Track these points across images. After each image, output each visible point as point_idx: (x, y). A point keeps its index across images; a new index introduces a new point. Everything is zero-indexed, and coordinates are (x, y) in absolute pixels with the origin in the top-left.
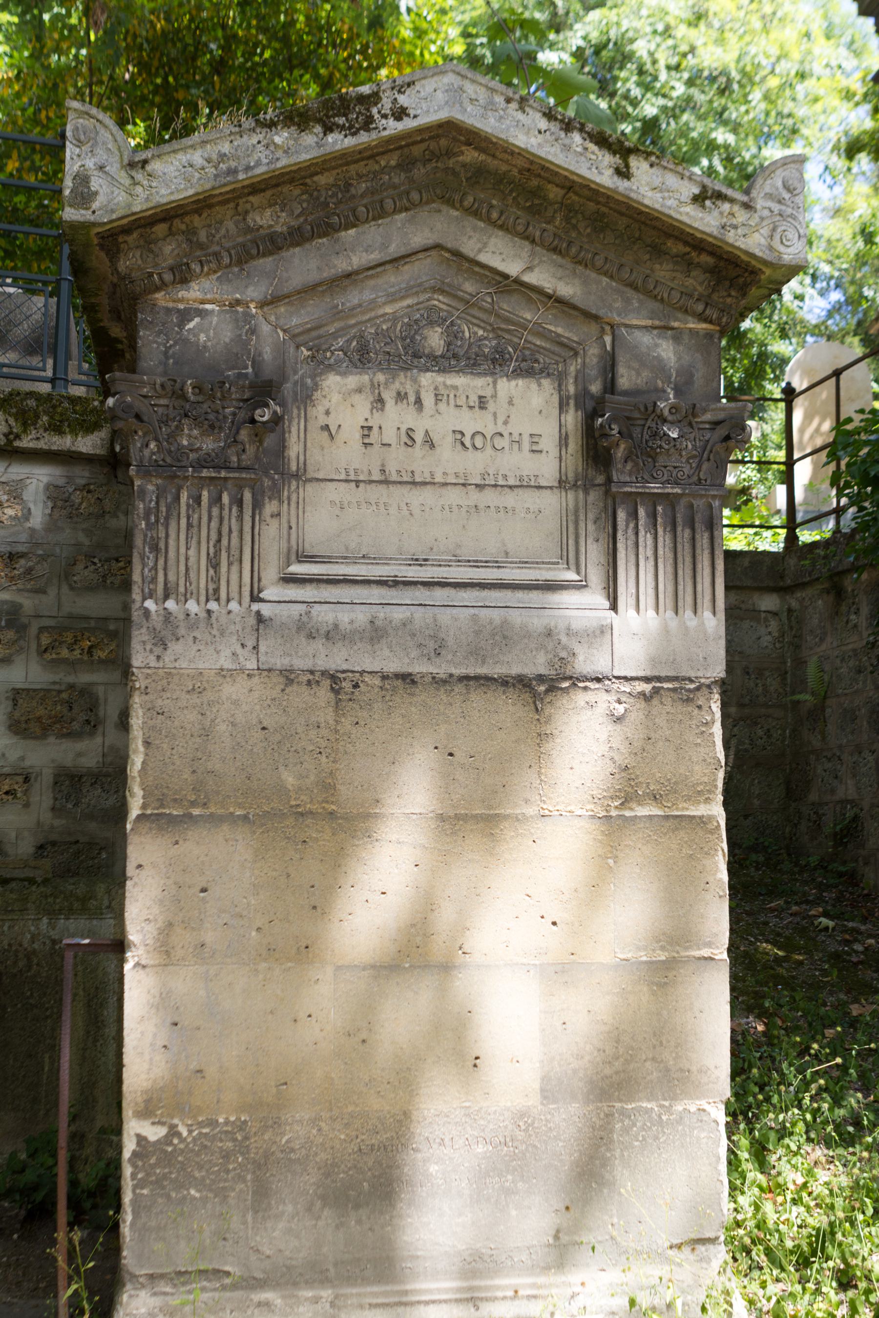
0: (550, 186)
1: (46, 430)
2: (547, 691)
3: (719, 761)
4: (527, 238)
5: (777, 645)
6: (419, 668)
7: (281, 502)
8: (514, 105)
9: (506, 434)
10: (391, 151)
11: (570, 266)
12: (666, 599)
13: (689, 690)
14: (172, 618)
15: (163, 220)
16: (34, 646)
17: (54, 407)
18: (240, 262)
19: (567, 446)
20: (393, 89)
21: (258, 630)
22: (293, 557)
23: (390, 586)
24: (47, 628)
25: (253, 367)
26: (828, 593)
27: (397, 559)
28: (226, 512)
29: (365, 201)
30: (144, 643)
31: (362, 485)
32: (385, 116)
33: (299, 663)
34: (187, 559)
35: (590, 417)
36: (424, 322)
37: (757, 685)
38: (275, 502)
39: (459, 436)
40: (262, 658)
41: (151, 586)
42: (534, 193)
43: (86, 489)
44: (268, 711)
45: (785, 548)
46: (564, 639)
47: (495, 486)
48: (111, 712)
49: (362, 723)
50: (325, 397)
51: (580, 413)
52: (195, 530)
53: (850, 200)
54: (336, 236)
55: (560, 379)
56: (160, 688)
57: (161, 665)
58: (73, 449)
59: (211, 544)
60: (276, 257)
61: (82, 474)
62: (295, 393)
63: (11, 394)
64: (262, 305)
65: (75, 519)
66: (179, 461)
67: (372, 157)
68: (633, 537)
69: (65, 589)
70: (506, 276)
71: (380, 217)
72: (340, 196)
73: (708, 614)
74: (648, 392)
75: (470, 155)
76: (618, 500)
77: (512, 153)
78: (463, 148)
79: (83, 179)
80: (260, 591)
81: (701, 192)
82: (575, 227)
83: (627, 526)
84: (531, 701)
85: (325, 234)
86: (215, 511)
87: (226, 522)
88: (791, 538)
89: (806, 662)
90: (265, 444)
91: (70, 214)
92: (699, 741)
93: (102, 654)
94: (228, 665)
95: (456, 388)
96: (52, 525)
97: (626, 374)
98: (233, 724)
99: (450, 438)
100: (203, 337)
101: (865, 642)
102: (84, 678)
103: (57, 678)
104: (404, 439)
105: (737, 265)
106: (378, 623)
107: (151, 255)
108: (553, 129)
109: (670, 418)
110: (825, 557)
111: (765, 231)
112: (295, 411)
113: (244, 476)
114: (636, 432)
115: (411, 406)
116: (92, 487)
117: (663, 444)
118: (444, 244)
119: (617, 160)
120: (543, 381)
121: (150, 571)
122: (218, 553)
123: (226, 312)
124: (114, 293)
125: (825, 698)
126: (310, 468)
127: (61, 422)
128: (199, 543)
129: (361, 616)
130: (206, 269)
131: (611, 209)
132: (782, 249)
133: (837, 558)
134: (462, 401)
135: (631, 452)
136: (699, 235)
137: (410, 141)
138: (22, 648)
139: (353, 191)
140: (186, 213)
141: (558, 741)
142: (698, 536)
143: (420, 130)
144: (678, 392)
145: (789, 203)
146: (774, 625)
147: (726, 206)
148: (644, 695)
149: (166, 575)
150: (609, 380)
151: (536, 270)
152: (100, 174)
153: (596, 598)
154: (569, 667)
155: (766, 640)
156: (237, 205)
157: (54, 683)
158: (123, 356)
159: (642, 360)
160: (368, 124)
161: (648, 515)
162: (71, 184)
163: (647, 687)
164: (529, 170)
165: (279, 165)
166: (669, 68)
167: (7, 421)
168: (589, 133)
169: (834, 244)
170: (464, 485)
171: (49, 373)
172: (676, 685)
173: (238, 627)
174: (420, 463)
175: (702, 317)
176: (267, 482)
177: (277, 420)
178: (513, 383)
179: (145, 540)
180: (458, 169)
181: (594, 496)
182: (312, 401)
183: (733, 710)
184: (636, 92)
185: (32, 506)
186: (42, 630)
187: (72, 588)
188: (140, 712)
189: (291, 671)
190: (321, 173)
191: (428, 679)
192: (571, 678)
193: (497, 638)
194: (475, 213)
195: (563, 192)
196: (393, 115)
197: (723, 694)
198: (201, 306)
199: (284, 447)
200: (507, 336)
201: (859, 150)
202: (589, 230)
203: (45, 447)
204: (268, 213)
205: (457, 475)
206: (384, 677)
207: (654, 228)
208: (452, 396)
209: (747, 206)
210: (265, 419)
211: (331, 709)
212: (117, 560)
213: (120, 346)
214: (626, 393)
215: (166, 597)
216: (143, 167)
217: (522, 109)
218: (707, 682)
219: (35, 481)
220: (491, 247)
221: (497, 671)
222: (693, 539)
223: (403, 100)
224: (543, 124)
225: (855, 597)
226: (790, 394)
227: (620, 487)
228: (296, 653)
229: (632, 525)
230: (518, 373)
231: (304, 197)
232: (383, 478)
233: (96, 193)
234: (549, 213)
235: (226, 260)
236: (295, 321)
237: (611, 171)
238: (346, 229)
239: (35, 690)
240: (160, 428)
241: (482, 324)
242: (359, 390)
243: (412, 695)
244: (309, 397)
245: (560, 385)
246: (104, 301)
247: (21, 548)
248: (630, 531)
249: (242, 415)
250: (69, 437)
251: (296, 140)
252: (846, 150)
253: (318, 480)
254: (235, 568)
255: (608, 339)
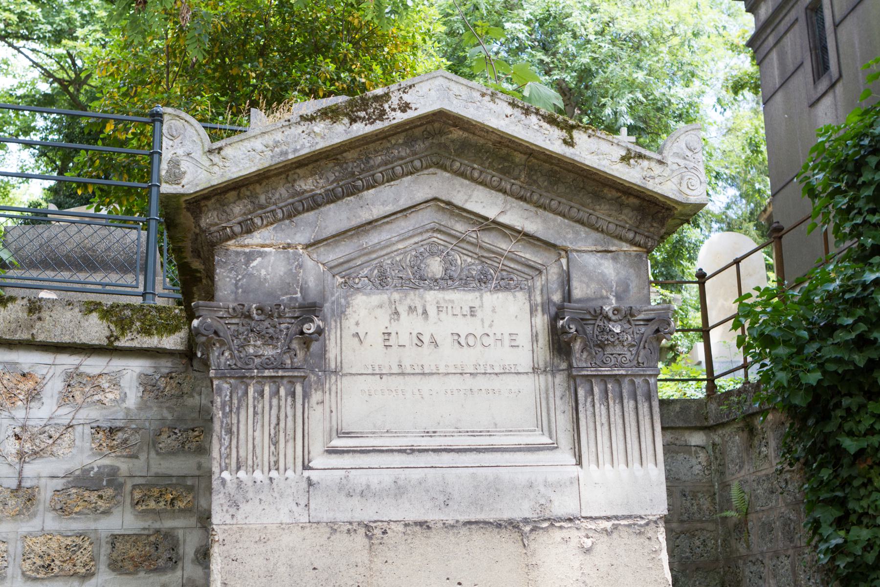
0: (516, 153)
1: (138, 333)
2: (532, 530)
3: (667, 580)
4: (500, 191)
5: (706, 472)
6: (430, 516)
7: (324, 392)
8: (487, 98)
9: (491, 334)
10: (399, 133)
11: (533, 209)
12: (619, 455)
13: (641, 526)
14: (243, 486)
15: (234, 189)
16: (128, 500)
17: (145, 315)
18: (290, 216)
19: (537, 341)
20: (399, 90)
21: (308, 492)
22: (334, 434)
23: (408, 454)
24: (138, 485)
25: (301, 293)
26: (743, 431)
27: (412, 433)
28: (283, 403)
29: (381, 169)
30: (222, 505)
31: (384, 377)
32: (394, 110)
33: (341, 517)
34: (254, 439)
35: (554, 320)
36: (427, 254)
37: (692, 505)
38: (319, 393)
39: (456, 337)
40: (312, 514)
41: (227, 461)
42: (505, 158)
43: (169, 376)
44: (318, 555)
45: (708, 396)
46: (542, 490)
47: (485, 373)
48: (189, 546)
49: (390, 562)
50: (355, 312)
51: (546, 316)
52: (259, 417)
53: (738, 122)
54: (360, 194)
55: (530, 291)
56: (234, 540)
57: (235, 521)
58: (160, 346)
59: (272, 426)
60: (317, 211)
61: (166, 365)
62: (333, 311)
63: (112, 307)
64: (307, 246)
65: (161, 400)
66: (247, 365)
67: (386, 138)
68: (591, 409)
69: (153, 454)
70: (486, 219)
71: (392, 180)
72: (362, 166)
73: (651, 466)
74: (596, 299)
75: (457, 134)
76: (578, 381)
77: (487, 132)
78: (452, 129)
79: (175, 163)
80: (309, 462)
81: (627, 154)
82: (535, 182)
83: (586, 401)
84: (519, 539)
85: (352, 194)
86: (275, 402)
87: (283, 409)
88: (711, 387)
89: (729, 485)
90: (311, 349)
91: (166, 188)
92: (651, 565)
93: (182, 505)
94: (286, 519)
95: (452, 301)
96: (143, 406)
97: (579, 287)
98: (291, 566)
99: (450, 339)
100: (263, 272)
101: (774, 469)
102: (168, 524)
103: (146, 525)
104: (416, 341)
105: (656, 205)
106: (400, 483)
107: (225, 214)
108: (516, 114)
109: (614, 318)
110: (739, 403)
111: (675, 180)
112: (333, 323)
113: (296, 374)
114: (589, 329)
115: (420, 316)
116: (173, 374)
117: (609, 337)
118: (440, 197)
119: (564, 134)
120: (517, 294)
121: (226, 449)
122: (277, 433)
123: (281, 253)
124: (196, 239)
125: (747, 514)
126: (345, 366)
127: (150, 326)
128: (263, 426)
129: (387, 477)
130: (265, 222)
131: (561, 167)
132: (688, 192)
133: (748, 403)
134: (457, 311)
135: (586, 345)
136: (627, 185)
137: (412, 125)
138: (119, 502)
139: (372, 162)
140: (251, 184)
141: (542, 569)
142: (640, 406)
143: (420, 118)
144: (618, 297)
145: (691, 159)
146: (702, 456)
147: (645, 163)
148: (606, 531)
149: (238, 452)
150: (566, 291)
151: (509, 213)
152: (188, 159)
153: (566, 456)
154: (547, 511)
155: (697, 469)
156: (288, 176)
157: (144, 529)
158: (201, 281)
159: (589, 276)
160: (382, 115)
161: (601, 391)
162: (166, 167)
163: (608, 525)
164: (500, 143)
165: (318, 147)
166: (596, 33)
167: (109, 327)
168: (542, 116)
169: (728, 154)
170: (461, 374)
171: (141, 289)
172: (631, 522)
173: (294, 490)
174: (427, 358)
175: (632, 243)
176: (313, 378)
177: (320, 332)
178: (495, 296)
179: (222, 426)
180: (448, 143)
181: (560, 378)
182: (345, 315)
183: (674, 525)
184: (572, 49)
185: (127, 390)
186: (134, 487)
187: (158, 454)
188: (219, 559)
189: (335, 523)
190: (349, 151)
191: (440, 525)
192: (549, 519)
193: (491, 490)
194: (463, 175)
195: (526, 157)
196: (400, 108)
197: (669, 531)
198: (262, 249)
199: (325, 351)
200: (489, 262)
201: (743, 87)
202: (546, 184)
203: (138, 346)
204: (310, 181)
205: (455, 367)
206: (406, 525)
207: (594, 180)
208: (450, 308)
209: (661, 162)
210: (311, 331)
211: (366, 552)
212: (193, 430)
213: (199, 275)
214: (579, 301)
215: (238, 469)
216: (219, 153)
217: (493, 100)
218: (654, 518)
219: (129, 371)
220: (474, 198)
221: (492, 516)
222: (637, 408)
223: (407, 98)
224: (509, 110)
225: (764, 433)
226: (702, 277)
227: (579, 371)
228: (338, 508)
229: (589, 400)
230: (498, 289)
231: (337, 168)
232: (400, 371)
233: (184, 173)
234: (516, 173)
235: (280, 215)
236: (332, 257)
237: (561, 141)
238: (368, 189)
239: (129, 535)
240: (233, 341)
241: (470, 254)
242: (381, 306)
243: (428, 537)
244: (343, 312)
245: (530, 297)
246: (188, 245)
247: (119, 424)
248: (588, 404)
249: (294, 329)
250: (156, 337)
251: (329, 129)
252: (732, 87)
253: (351, 374)
254: (290, 444)
255: (564, 261)
